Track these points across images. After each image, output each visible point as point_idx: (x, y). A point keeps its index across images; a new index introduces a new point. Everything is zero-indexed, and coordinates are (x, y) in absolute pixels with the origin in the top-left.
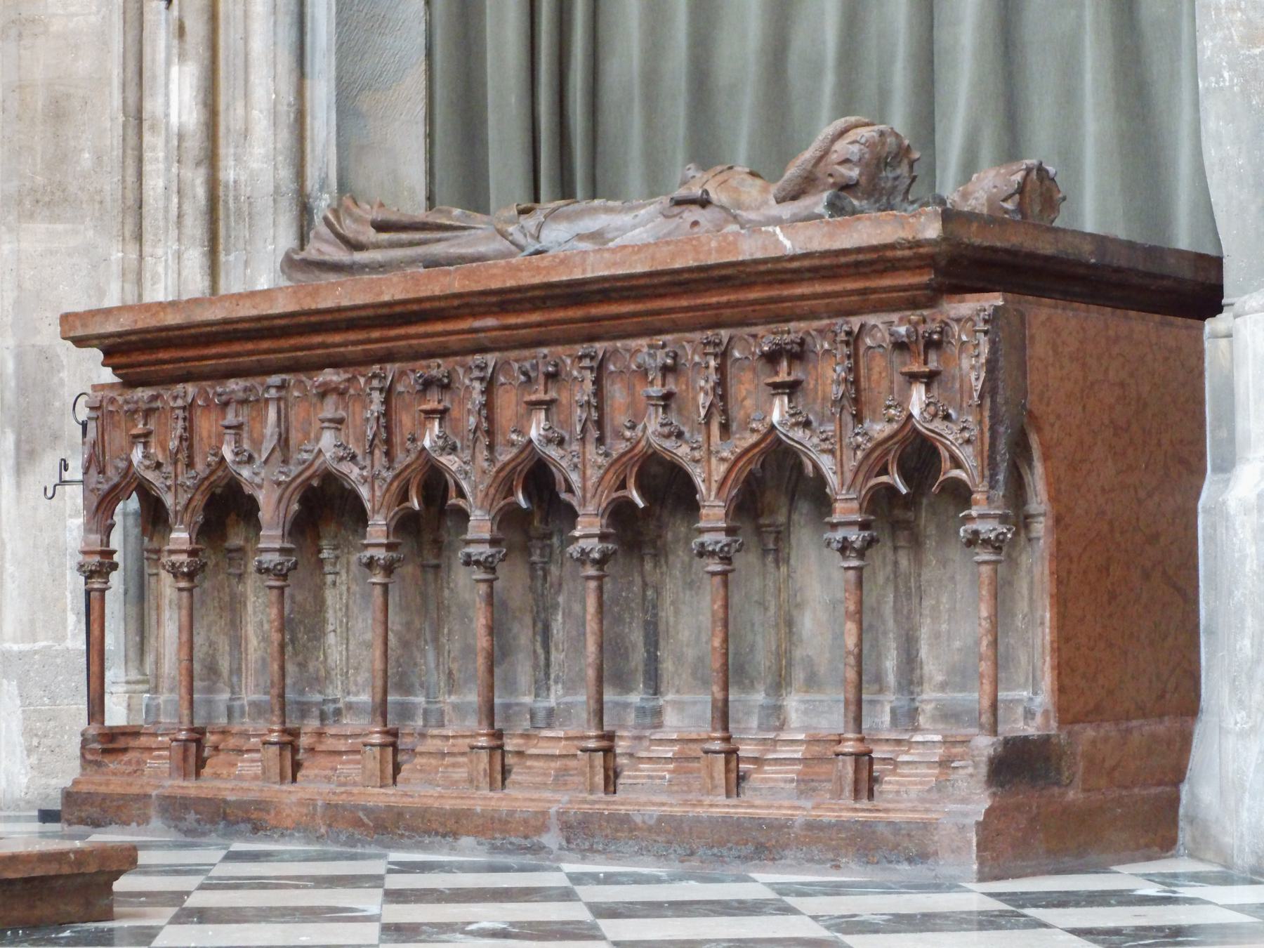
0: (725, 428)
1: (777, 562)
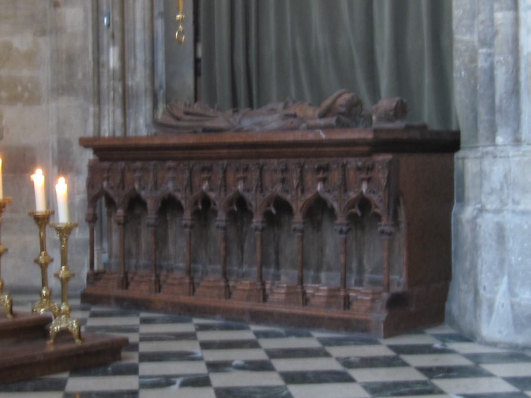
0: (303, 191)
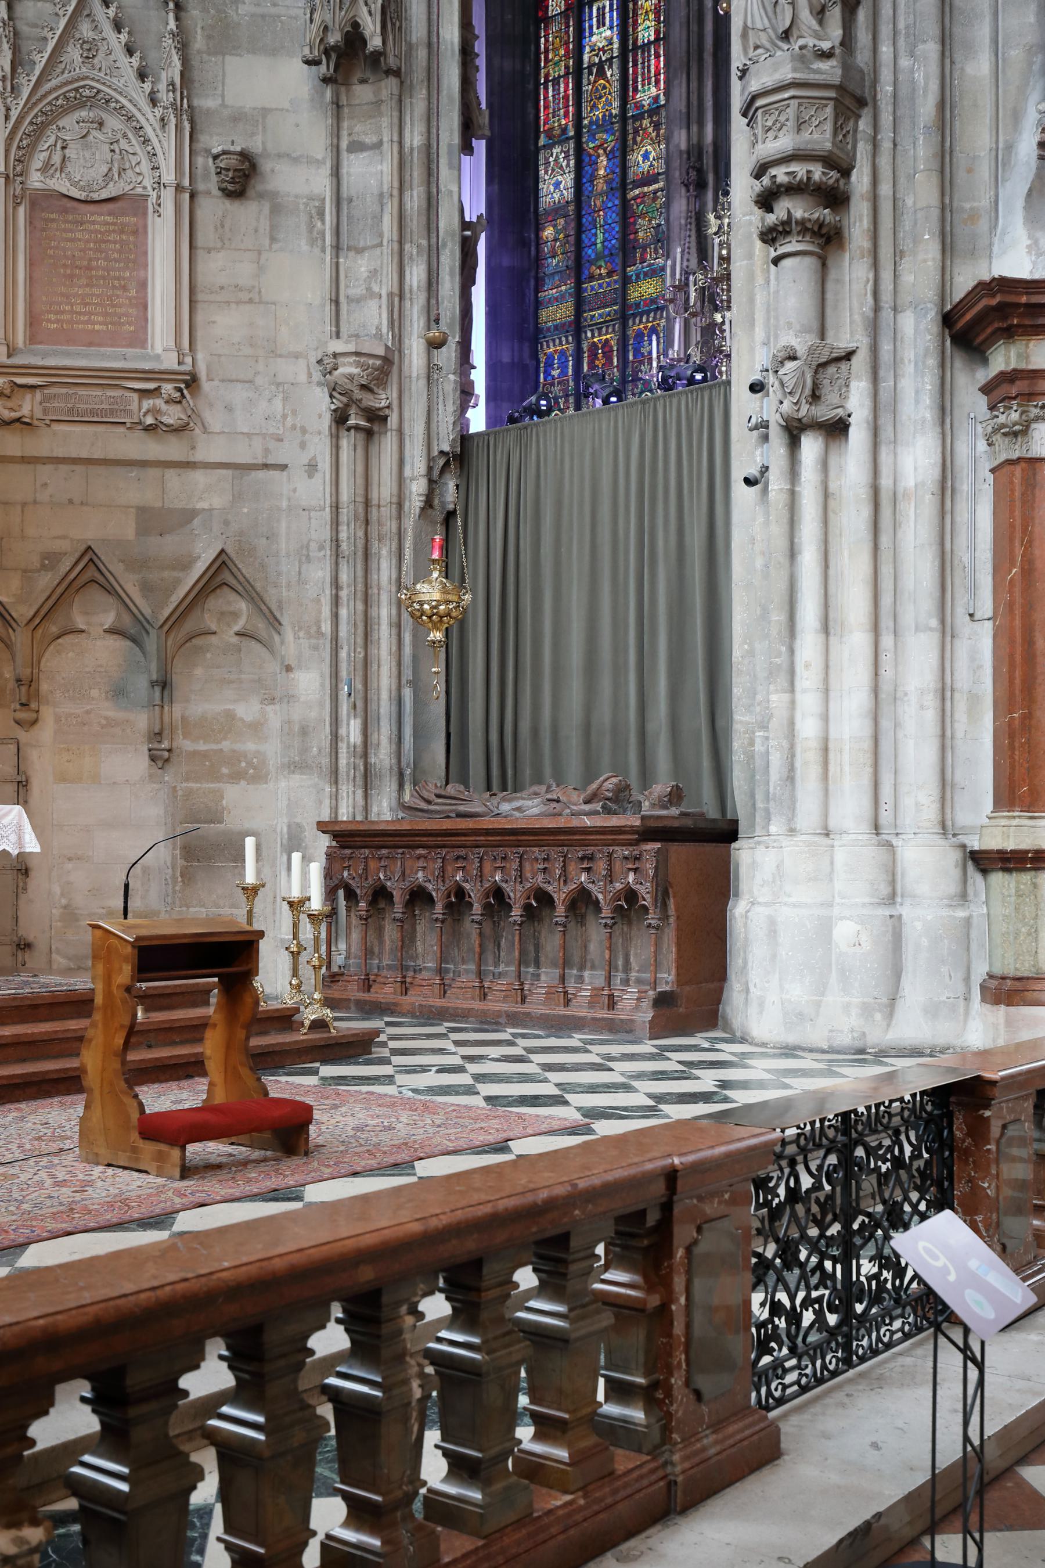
0: (565, 882)
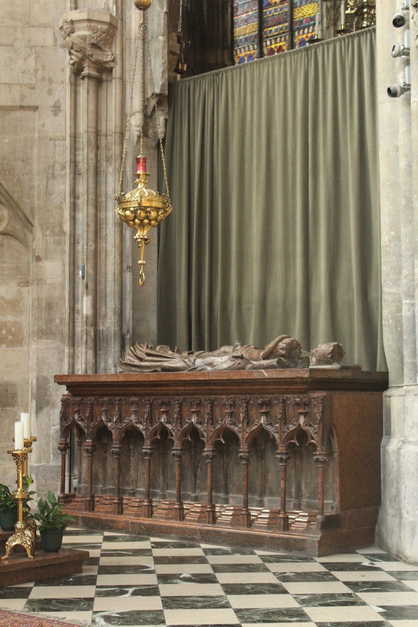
0: (248, 424)
1: (262, 460)
